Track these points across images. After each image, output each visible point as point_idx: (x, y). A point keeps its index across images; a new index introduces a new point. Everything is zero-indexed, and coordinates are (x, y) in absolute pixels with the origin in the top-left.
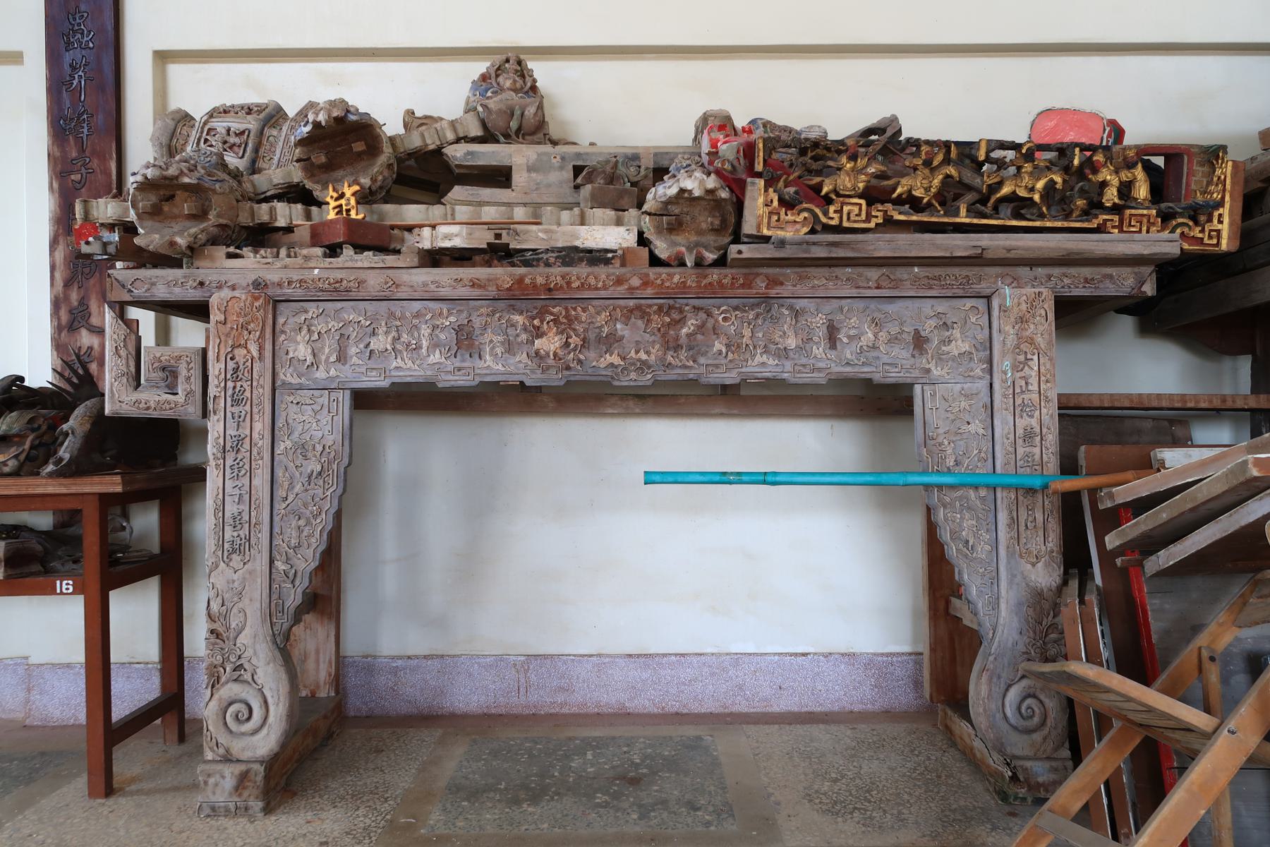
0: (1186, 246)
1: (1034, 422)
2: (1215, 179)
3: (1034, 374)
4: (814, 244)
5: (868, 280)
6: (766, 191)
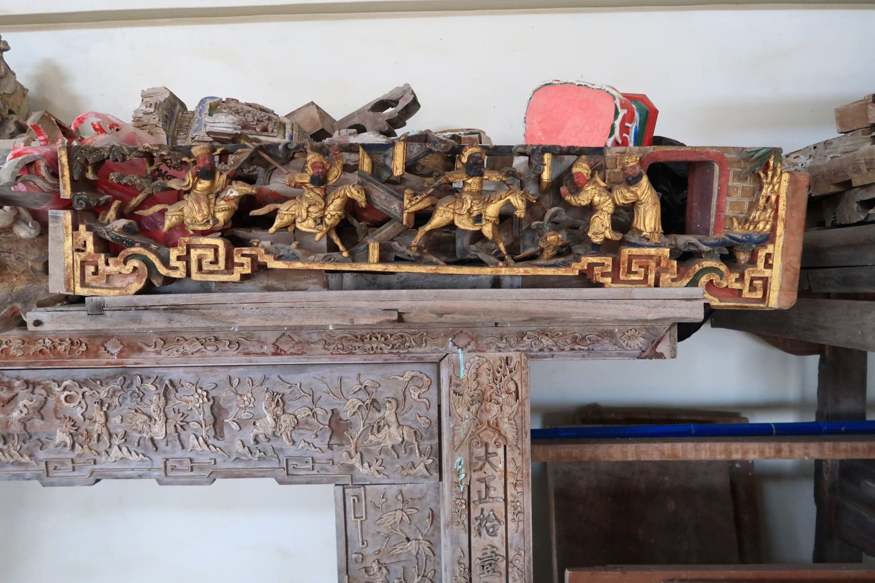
0: (715, 302)
1: (498, 541)
2: (762, 201)
3: (499, 474)
4: (146, 308)
5: (262, 343)
6: (75, 228)
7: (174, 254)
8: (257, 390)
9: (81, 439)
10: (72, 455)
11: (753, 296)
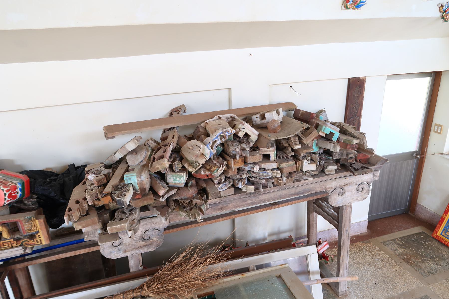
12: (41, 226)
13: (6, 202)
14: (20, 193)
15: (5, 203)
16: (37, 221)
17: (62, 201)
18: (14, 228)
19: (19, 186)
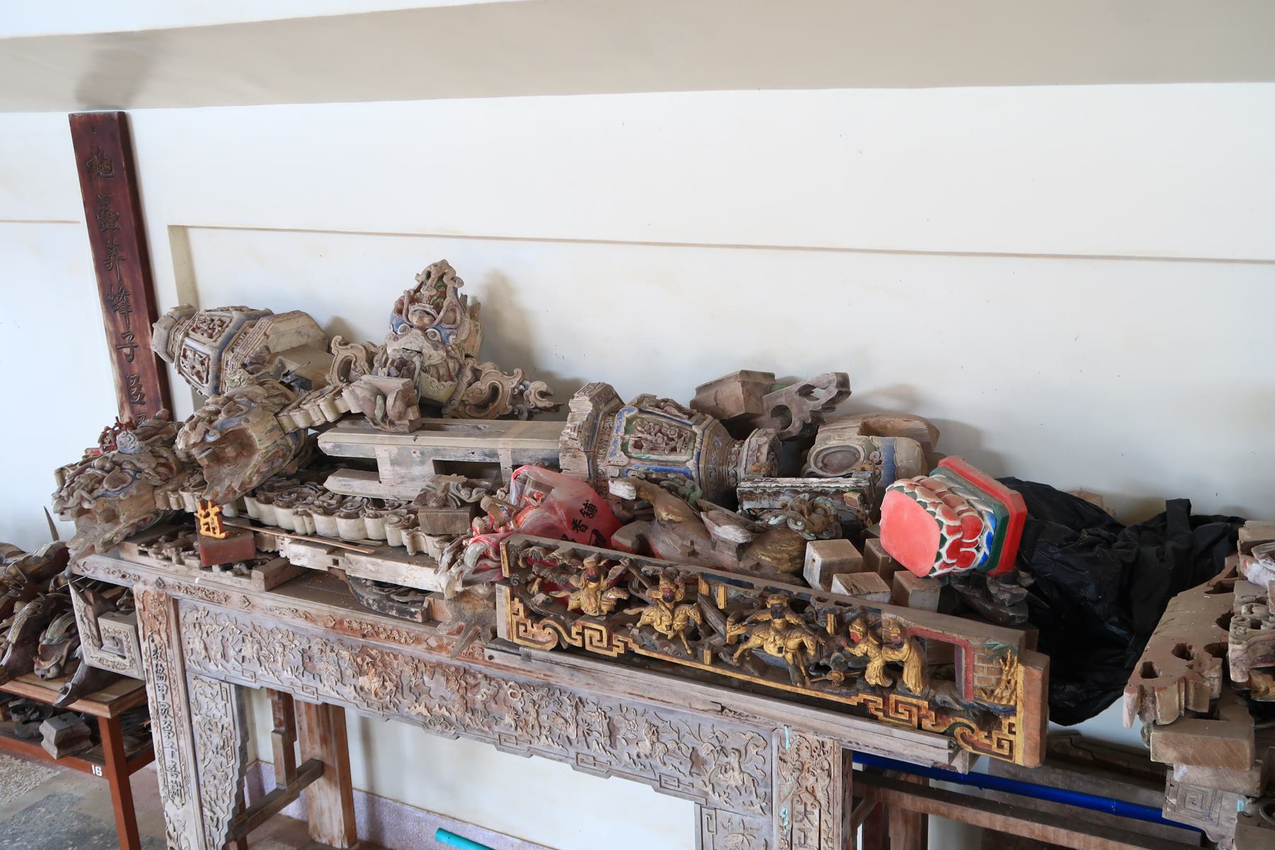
4: (557, 664)
6: (512, 599)
7: (574, 630)
8: (639, 718)
9: (522, 724)
10: (515, 734)
11: (1000, 751)
12: (1027, 693)
13: (936, 565)
14: (985, 549)
15: (933, 570)
16: (1021, 668)
17: (1114, 629)
18: (941, 666)
19: (989, 526)
